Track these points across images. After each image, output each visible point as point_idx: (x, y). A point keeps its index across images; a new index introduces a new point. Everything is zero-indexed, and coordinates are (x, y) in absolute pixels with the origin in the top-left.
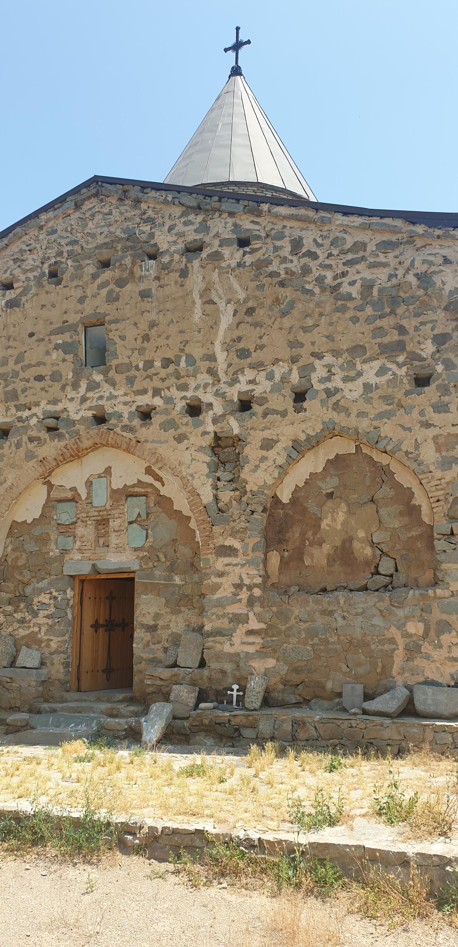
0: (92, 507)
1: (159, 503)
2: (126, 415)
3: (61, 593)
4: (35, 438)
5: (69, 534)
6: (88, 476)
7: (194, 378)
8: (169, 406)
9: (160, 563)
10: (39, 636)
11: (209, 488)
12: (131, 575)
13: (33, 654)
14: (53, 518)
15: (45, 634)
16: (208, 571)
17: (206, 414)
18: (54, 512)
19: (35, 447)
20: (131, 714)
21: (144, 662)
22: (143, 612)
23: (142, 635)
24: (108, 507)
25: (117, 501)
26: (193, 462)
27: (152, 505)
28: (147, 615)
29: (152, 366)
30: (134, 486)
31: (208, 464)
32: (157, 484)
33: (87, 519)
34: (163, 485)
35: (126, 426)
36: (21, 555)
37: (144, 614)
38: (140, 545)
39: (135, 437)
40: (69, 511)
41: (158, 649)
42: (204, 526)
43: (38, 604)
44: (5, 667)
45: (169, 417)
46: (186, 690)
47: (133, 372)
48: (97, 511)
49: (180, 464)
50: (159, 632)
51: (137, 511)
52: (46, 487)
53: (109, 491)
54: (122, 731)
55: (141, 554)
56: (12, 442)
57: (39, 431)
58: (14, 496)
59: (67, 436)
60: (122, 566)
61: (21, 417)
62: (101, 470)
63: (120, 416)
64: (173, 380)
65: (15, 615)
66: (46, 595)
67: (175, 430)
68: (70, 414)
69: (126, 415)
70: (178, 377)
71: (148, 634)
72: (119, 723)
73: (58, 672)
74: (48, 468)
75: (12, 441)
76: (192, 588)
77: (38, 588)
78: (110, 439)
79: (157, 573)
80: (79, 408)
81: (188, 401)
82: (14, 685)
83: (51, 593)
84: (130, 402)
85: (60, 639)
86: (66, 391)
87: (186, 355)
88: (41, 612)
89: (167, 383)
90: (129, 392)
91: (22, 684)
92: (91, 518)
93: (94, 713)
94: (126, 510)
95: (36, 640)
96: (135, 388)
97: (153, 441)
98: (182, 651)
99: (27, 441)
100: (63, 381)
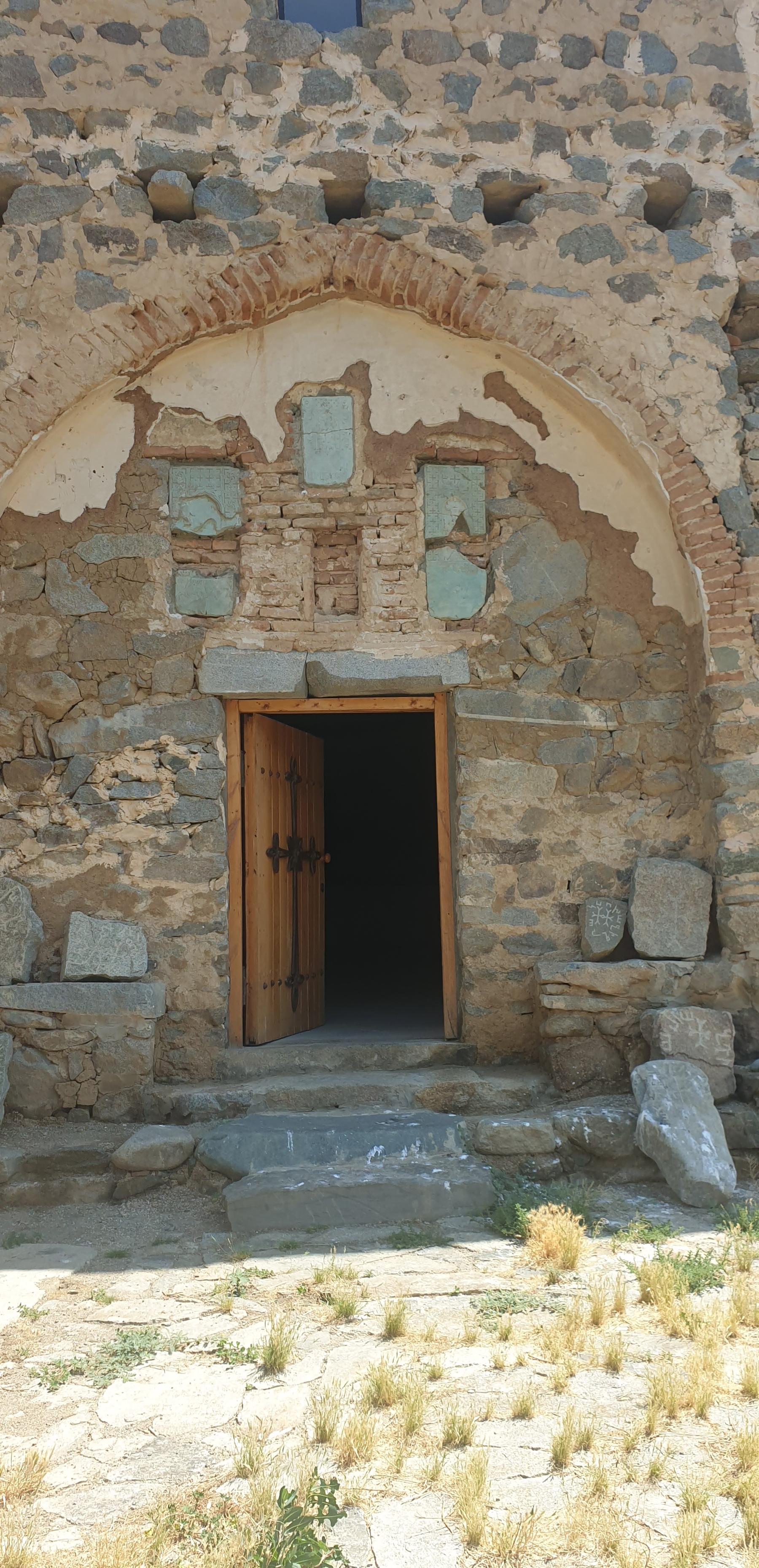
0: (302, 485)
1: (530, 488)
2: (444, 199)
3: (195, 748)
4: (115, 231)
5: (212, 569)
6: (287, 385)
7: (666, 113)
8: (589, 186)
9: (534, 668)
10: (125, 880)
11: (730, 445)
12: (424, 704)
13: (121, 934)
14: (156, 512)
15: (148, 874)
16: (734, 685)
17: (710, 226)
18: (159, 494)
19: (112, 261)
20: (508, 1102)
21: (499, 947)
22: (487, 807)
23: (490, 871)
24: (358, 488)
25: (390, 471)
26: (678, 362)
27: (503, 493)
28: (502, 816)
29: (529, 55)
30: (446, 429)
31: (723, 374)
32: (526, 431)
33: (284, 523)
34: (544, 434)
35: (447, 230)
36: (42, 625)
37: (491, 813)
38: (469, 611)
39: (478, 270)
40: (217, 494)
41: (544, 911)
42: (716, 555)
43: (109, 780)
44: (14, 982)
45: (593, 220)
46: (701, 1023)
47: (466, 65)
48: (320, 500)
49: (634, 363)
50: (542, 862)
51: (456, 507)
52: (128, 411)
53: (360, 440)
54: (546, 1154)
55: (474, 639)
56: (23, 234)
57: (128, 212)
58: (40, 419)
59: (233, 238)
60: (411, 673)
61: (54, 155)
62: (334, 371)
63: (426, 197)
64: (601, 108)
65: (24, 815)
66: (141, 755)
67: (614, 262)
68: (244, 169)
69: (444, 199)
70: (619, 102)
71: (509, 868)
72: (536, 1133)
73: (200, 986)
74: (161, 337)
75: (22, 231)
76: (643, 738)
77: (110, 732)
78: (386, 268)
79: (528, 694)
80: (273, 154)
81: (651, 180)
82: (69, 1035)
83: (160, 749)
84: (455, 158)
85: (203, 888)
86: (225, 90)
87: (644, 37)
88: (125, 806)
89: (581, 115)
90: (453, 123)
91: (100, 1030)
92: (298, 522)
93: (389, 1104)
94: (419, 503)
95: (113, 893)
96: (475, 115)
97: (540, 288)
98: (644, 914)
99: (83, 239)
100: (214, 57)
